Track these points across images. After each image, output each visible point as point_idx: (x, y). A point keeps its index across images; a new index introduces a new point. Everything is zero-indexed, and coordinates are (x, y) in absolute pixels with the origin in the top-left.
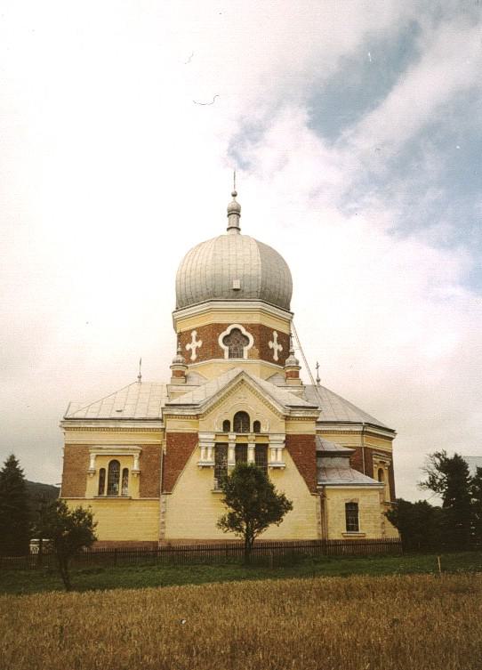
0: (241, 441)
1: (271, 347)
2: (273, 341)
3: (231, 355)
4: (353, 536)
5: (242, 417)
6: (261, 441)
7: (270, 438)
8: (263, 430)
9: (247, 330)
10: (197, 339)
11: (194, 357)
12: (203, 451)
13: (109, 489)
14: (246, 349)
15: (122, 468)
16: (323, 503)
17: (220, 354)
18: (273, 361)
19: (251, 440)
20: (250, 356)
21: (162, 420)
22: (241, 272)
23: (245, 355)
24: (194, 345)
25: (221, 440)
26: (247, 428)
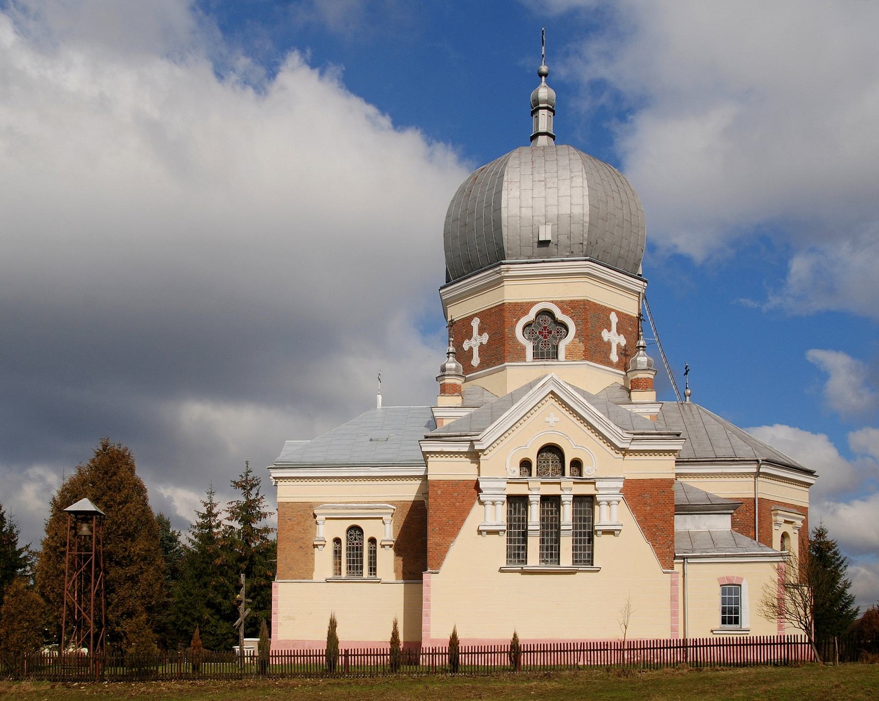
1: (606, 339)
2: (609, 330)
3: (537, 356)
4: (730, 633)
7: (598, 484)
8: (588, 471)
9: (564, 311)
11: (476, 361)
14: (563, 345)
15: (366, 537)
16: (479, 468)
17: (520, 355)
18: (609, 363)
19: (567, 489)
20: (570, 355)
21: (425, 454)
22: (553, 212)
23: (562, 354)
24: (476, 341)
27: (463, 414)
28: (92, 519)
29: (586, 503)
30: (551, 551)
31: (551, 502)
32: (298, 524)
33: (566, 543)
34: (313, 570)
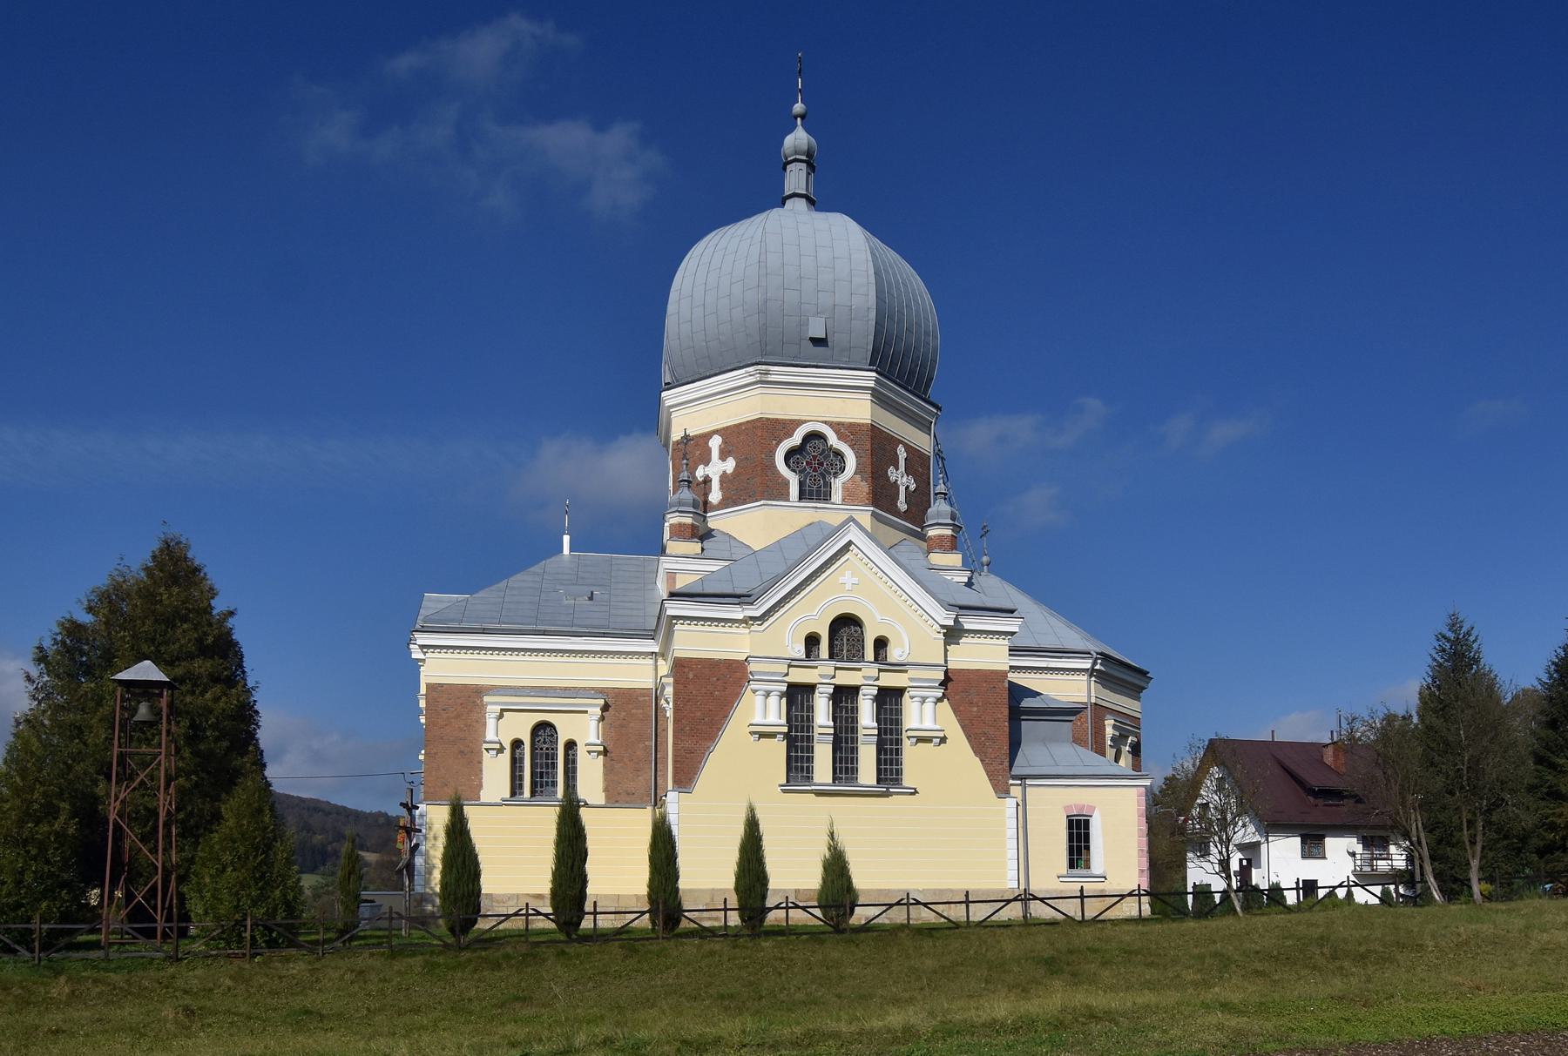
0: (845, 679)
1: (893, 479)
5: (846, 625)
6: (890, 680)
8: (895, 654)
9: (841, 437)
10: (723, 456)
12: (759, 699)
13: (534, 784)
14: (837, 485)
17: (777, 491)
19: (864, 676)
20: (849, 497)
23: (837, 496)
25: (800, 676)
26: (857, 654)
27: (715, 569)
28: (161, 695)
29: (889, 699)
30: (844, 765)
31: (844, 697)
32: (458, 716)
33: (867, 757)
34: (480, 786)
